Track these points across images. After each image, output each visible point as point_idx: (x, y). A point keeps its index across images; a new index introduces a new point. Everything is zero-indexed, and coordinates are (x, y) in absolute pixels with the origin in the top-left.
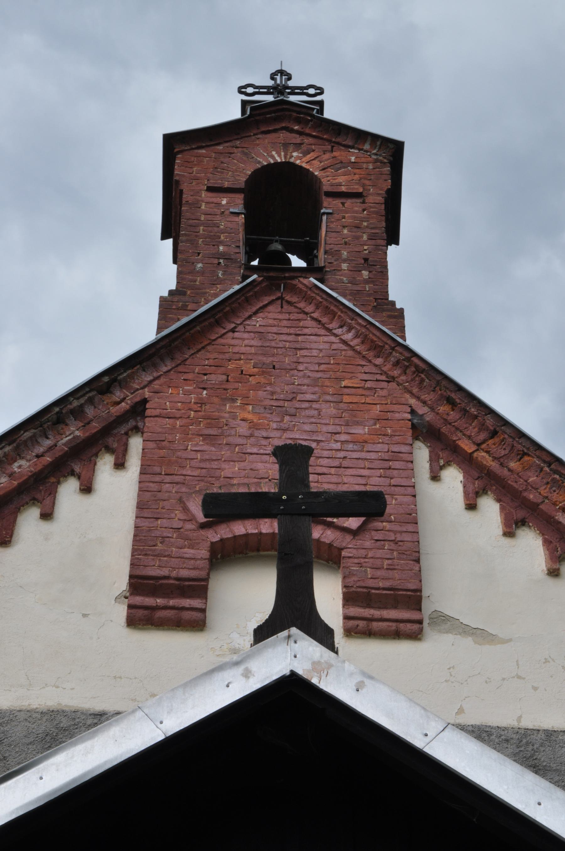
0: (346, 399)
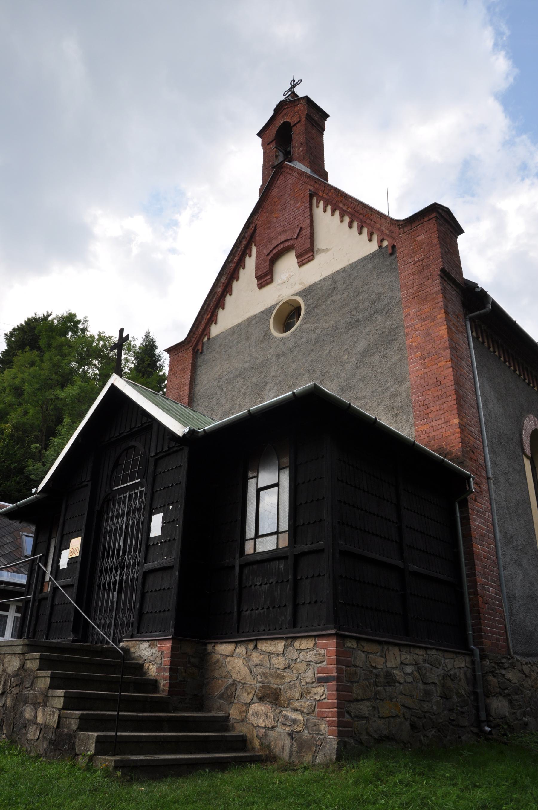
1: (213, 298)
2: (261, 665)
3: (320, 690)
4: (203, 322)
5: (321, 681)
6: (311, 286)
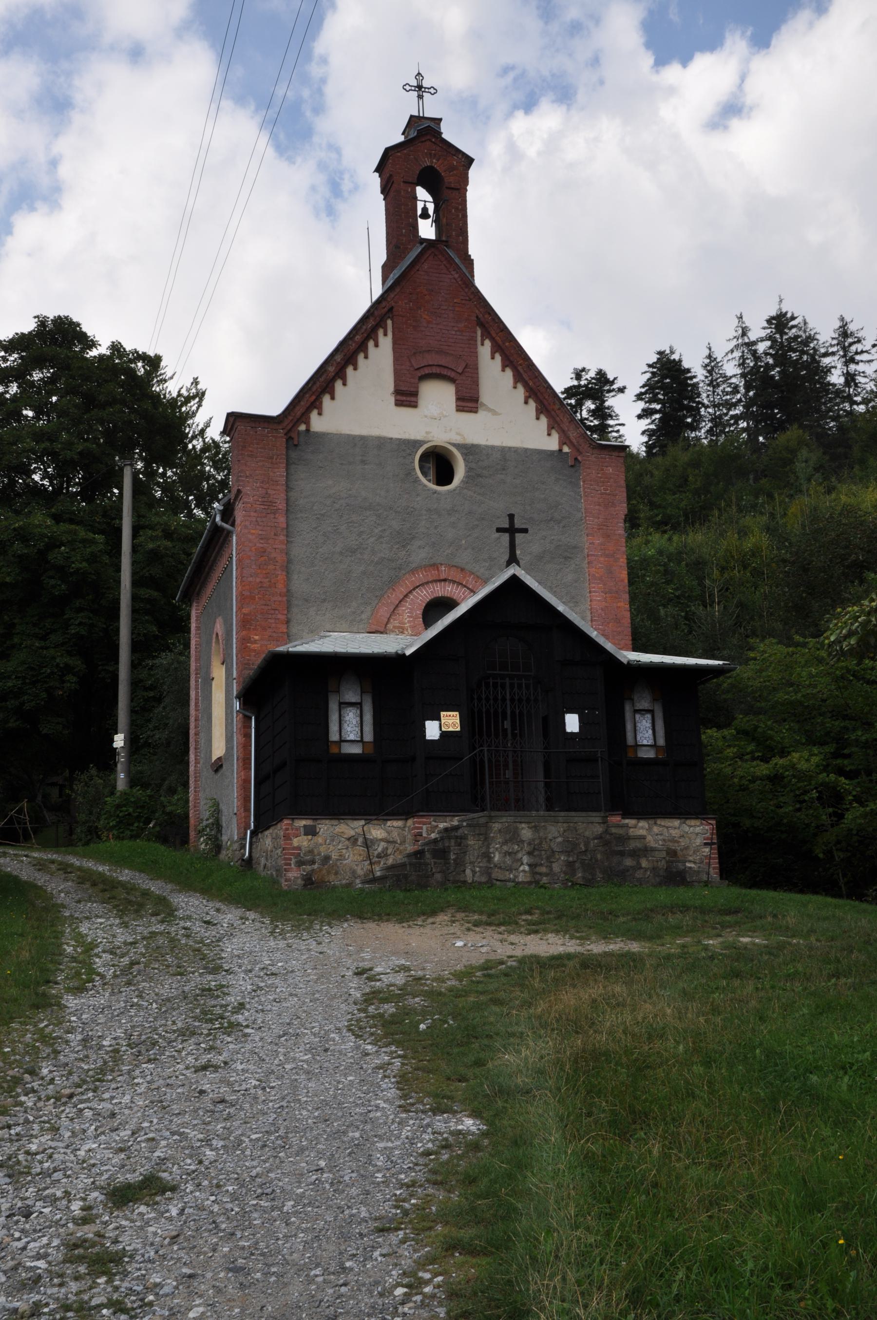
0: (457, 309)
1: (320, 377)
2: (661, 835)
4: (302, 403)
6: (473, 446)
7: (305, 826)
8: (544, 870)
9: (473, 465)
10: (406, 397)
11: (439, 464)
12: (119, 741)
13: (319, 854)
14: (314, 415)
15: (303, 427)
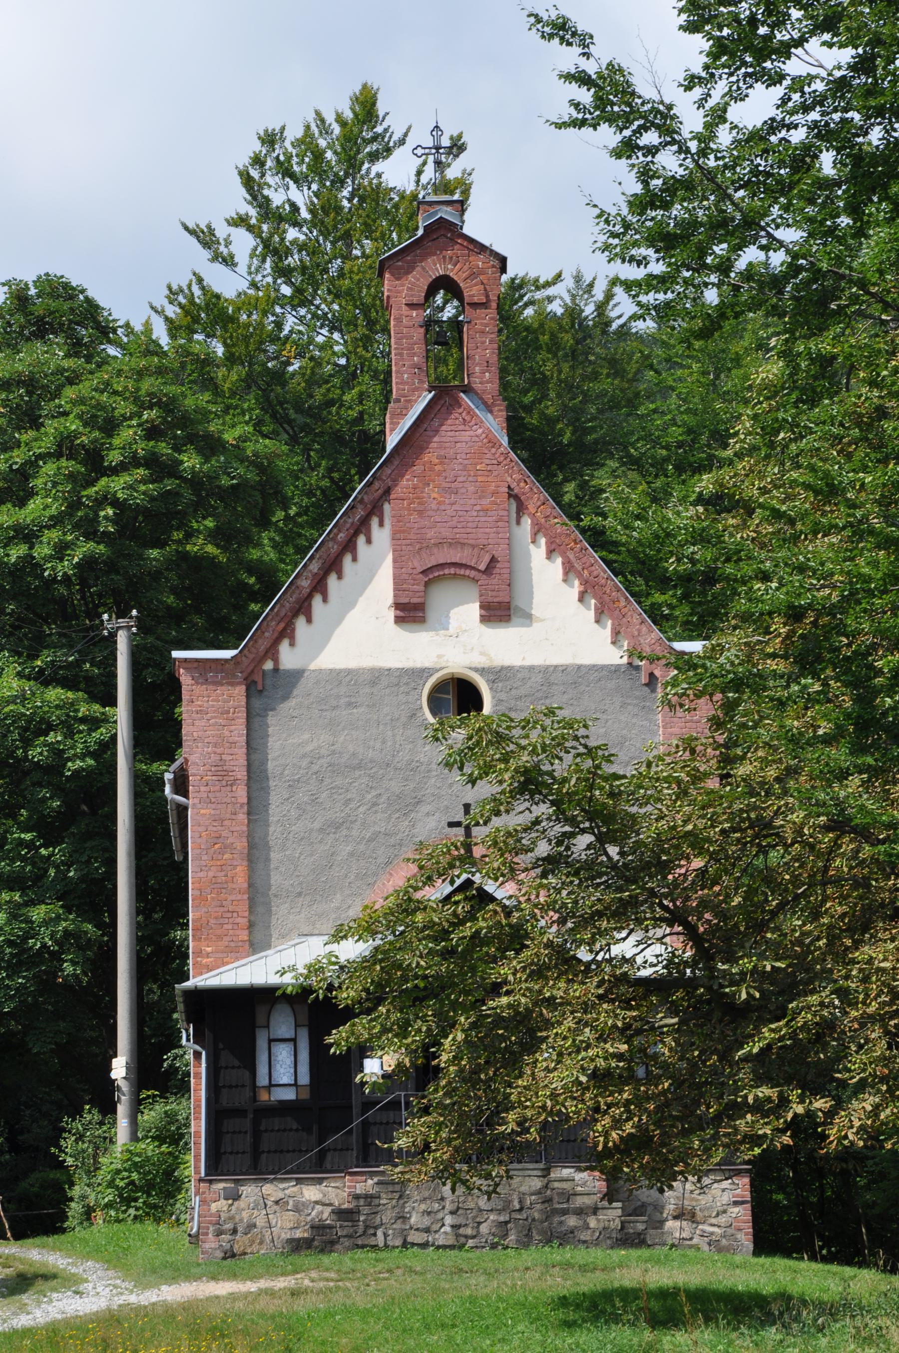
0: (480, 479)
3: (736, 1210)
5: (736, 1203)
6: (503, 668)
7: (224, 1189)
8: (469, 1231)
9: (503, 696)
10: (410, 612)
11: (460, 695)
12: (119, 1069)
13: (241, 1220)
14: (284, 647)
15: (269, 665)
